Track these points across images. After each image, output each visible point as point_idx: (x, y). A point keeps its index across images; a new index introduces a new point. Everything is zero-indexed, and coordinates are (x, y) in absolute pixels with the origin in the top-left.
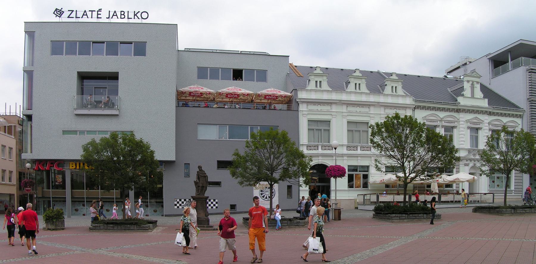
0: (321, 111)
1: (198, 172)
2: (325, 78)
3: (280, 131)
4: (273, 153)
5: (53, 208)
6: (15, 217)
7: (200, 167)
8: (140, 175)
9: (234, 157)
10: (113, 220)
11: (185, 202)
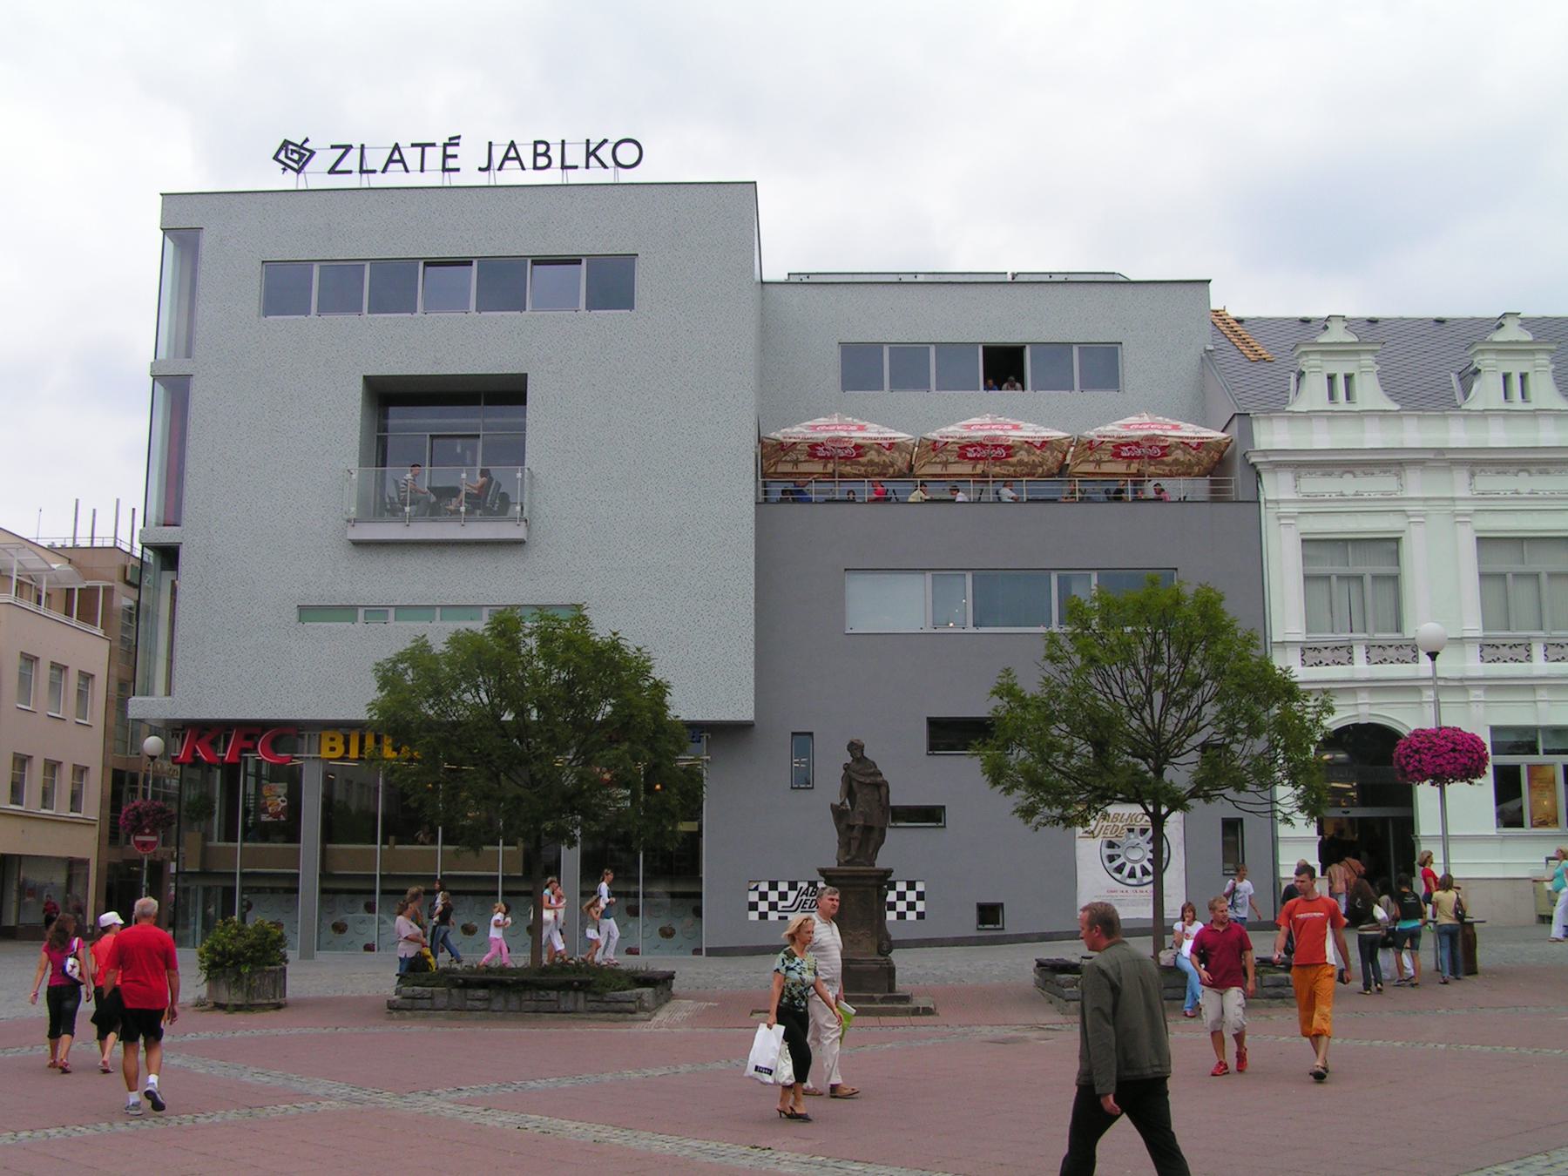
0: (1358, 497)
1: (847, 767)
2: (1368, 360)
3: (1189, 591)
4: (1162, 682)
5: (243, 919)
6: (85, 953)
7: (855, 748)
8: (610, 784)
9: (996, 701)
10: (489, 970)
11: (792, 895)
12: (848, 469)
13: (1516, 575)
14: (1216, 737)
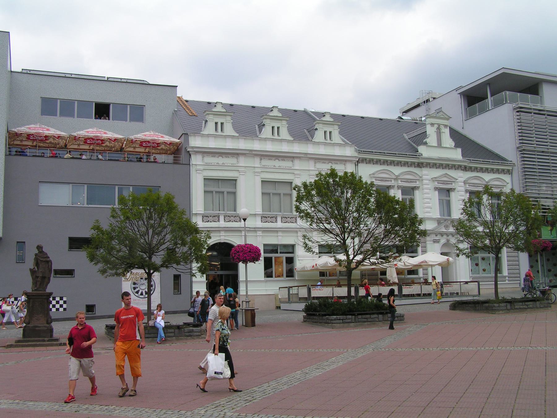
0: (279, 167)
1: (36, 255)
2: (229, 118)
3: (163, 194)
4: (152, 226)
7: (39, 248)
9: (93, 231)
12: (42, 144)
13: (273, 194)
14: (170, 246)
